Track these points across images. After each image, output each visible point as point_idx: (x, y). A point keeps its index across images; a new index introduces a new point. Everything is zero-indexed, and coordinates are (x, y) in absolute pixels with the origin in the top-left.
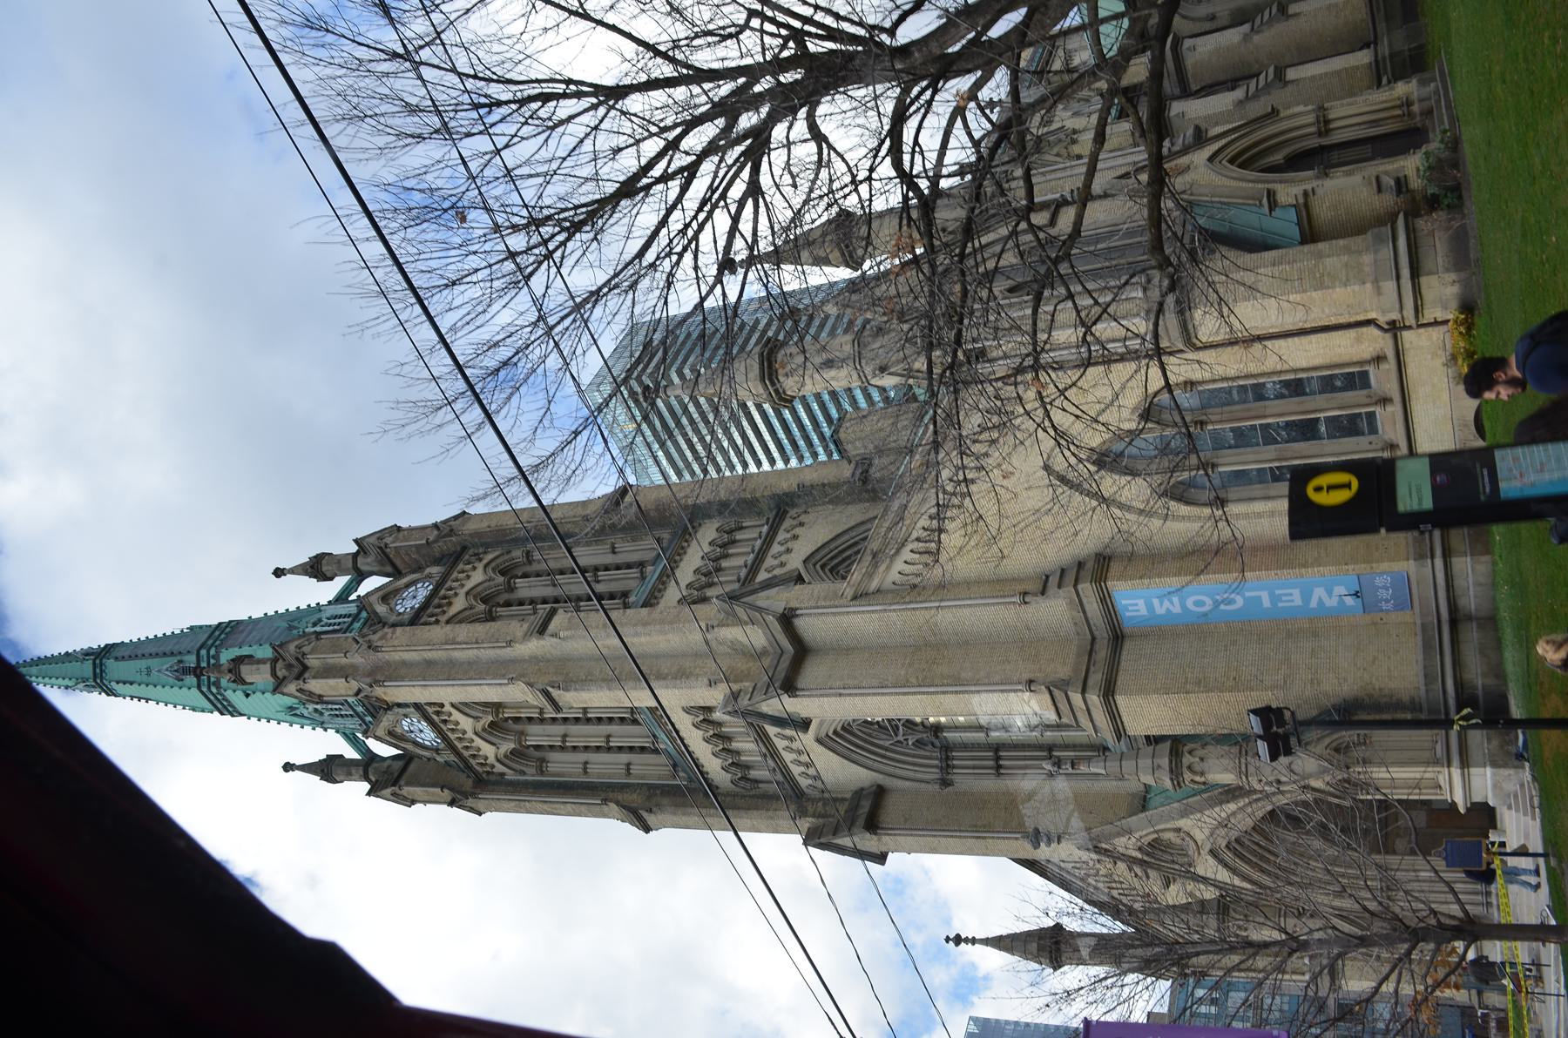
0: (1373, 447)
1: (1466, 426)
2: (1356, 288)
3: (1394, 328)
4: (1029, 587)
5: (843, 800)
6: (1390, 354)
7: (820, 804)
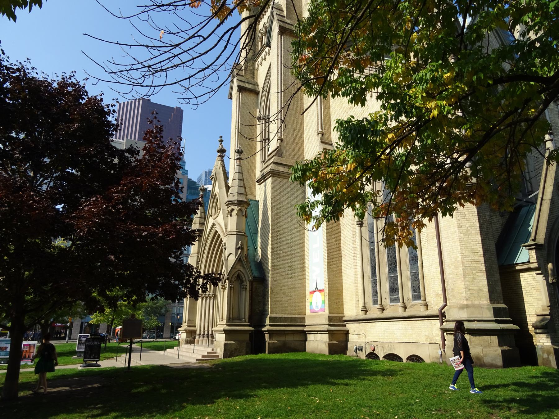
0: (383, 300)
1: (391, 349)
2: (464, 295)
3: (442, 316)
4: (326, 136)
5: (253, 78)
6: (428, 313)
7: (251, 68)
